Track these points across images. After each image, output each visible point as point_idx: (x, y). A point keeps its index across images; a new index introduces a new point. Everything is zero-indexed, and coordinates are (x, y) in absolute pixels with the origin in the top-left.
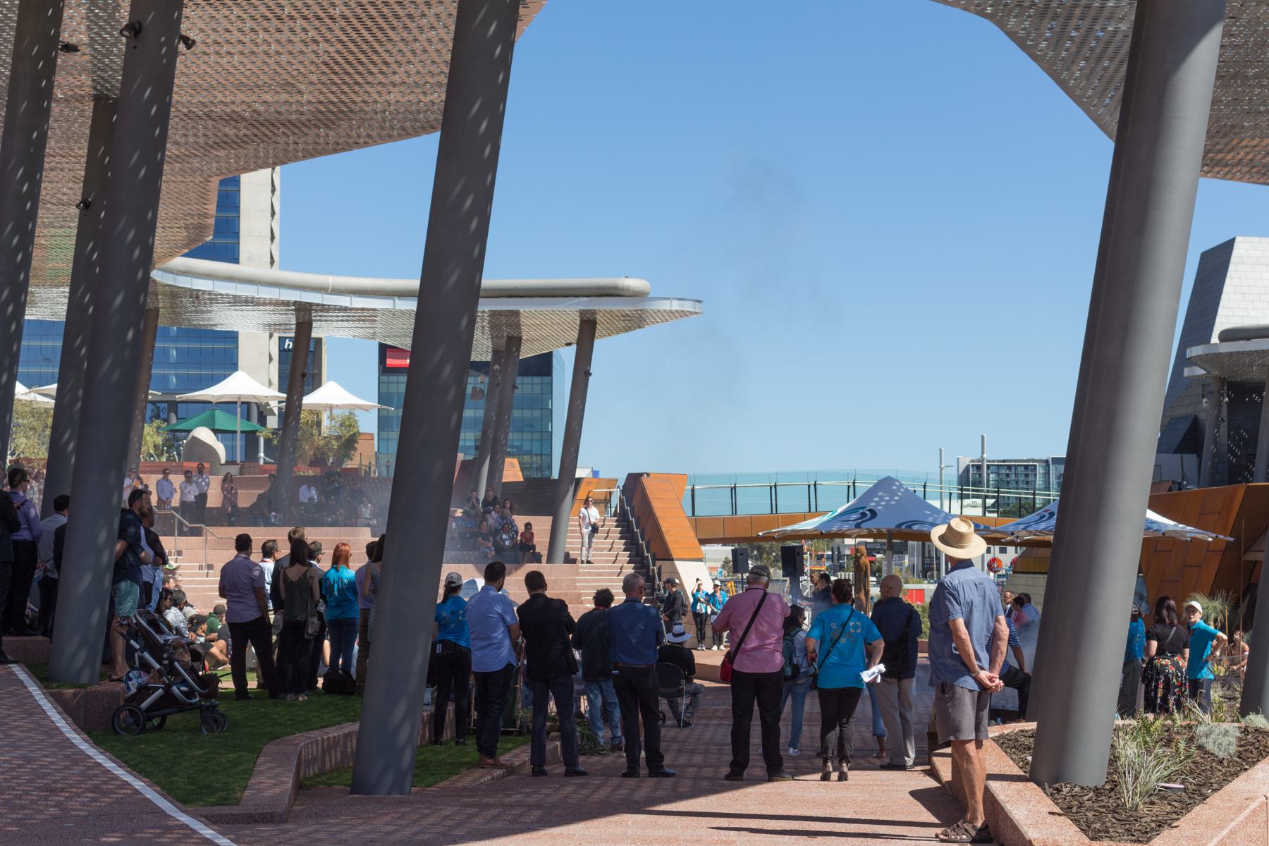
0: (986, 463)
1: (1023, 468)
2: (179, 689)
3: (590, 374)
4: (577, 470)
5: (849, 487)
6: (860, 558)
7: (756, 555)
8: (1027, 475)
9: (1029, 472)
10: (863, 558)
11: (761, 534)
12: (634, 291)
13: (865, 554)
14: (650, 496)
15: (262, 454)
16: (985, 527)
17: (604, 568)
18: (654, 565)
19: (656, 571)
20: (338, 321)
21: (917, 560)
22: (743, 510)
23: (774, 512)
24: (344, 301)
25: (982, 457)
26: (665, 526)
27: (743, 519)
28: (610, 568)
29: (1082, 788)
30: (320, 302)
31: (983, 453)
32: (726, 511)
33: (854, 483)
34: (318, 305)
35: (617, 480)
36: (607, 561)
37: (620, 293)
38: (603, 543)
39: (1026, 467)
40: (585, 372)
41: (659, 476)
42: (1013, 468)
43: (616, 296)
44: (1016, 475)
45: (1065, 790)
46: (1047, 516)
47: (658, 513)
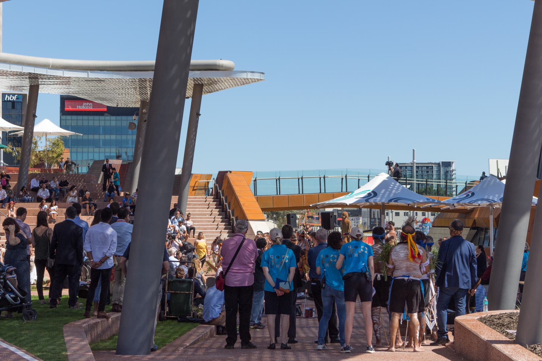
0: (415, 165)
1: (425, 168)
2: (10, 296)
3: (200, 115)
4: (176, 169)
5: (342, 179)
6: (345, 219)
8: (428, 172)
9: (429, 170)
10: (347, 218)
11: (311, 205)
12: (225, 67)
13: (348, 216)
14: (233, 184)
15: (2, 161)
17: (207, 225)
20: (54, 84)
22: (283, 193)
23: (278, 194)
24: (59, 73)
25: (413, 161)
26: (242, 201)
27: (284, 197)
28: (211, 225)
31: (414, 159)
32: (273, 192)
33: (346, 176)
34: (44, 75)
35: (211, 175)
36: (209, 221)
37: (218, 68)
38: (206, 211)
39: (427, 167)
40: (197, 113)
41: (236, 172)
42: (420, 167)
44: (422, 171)
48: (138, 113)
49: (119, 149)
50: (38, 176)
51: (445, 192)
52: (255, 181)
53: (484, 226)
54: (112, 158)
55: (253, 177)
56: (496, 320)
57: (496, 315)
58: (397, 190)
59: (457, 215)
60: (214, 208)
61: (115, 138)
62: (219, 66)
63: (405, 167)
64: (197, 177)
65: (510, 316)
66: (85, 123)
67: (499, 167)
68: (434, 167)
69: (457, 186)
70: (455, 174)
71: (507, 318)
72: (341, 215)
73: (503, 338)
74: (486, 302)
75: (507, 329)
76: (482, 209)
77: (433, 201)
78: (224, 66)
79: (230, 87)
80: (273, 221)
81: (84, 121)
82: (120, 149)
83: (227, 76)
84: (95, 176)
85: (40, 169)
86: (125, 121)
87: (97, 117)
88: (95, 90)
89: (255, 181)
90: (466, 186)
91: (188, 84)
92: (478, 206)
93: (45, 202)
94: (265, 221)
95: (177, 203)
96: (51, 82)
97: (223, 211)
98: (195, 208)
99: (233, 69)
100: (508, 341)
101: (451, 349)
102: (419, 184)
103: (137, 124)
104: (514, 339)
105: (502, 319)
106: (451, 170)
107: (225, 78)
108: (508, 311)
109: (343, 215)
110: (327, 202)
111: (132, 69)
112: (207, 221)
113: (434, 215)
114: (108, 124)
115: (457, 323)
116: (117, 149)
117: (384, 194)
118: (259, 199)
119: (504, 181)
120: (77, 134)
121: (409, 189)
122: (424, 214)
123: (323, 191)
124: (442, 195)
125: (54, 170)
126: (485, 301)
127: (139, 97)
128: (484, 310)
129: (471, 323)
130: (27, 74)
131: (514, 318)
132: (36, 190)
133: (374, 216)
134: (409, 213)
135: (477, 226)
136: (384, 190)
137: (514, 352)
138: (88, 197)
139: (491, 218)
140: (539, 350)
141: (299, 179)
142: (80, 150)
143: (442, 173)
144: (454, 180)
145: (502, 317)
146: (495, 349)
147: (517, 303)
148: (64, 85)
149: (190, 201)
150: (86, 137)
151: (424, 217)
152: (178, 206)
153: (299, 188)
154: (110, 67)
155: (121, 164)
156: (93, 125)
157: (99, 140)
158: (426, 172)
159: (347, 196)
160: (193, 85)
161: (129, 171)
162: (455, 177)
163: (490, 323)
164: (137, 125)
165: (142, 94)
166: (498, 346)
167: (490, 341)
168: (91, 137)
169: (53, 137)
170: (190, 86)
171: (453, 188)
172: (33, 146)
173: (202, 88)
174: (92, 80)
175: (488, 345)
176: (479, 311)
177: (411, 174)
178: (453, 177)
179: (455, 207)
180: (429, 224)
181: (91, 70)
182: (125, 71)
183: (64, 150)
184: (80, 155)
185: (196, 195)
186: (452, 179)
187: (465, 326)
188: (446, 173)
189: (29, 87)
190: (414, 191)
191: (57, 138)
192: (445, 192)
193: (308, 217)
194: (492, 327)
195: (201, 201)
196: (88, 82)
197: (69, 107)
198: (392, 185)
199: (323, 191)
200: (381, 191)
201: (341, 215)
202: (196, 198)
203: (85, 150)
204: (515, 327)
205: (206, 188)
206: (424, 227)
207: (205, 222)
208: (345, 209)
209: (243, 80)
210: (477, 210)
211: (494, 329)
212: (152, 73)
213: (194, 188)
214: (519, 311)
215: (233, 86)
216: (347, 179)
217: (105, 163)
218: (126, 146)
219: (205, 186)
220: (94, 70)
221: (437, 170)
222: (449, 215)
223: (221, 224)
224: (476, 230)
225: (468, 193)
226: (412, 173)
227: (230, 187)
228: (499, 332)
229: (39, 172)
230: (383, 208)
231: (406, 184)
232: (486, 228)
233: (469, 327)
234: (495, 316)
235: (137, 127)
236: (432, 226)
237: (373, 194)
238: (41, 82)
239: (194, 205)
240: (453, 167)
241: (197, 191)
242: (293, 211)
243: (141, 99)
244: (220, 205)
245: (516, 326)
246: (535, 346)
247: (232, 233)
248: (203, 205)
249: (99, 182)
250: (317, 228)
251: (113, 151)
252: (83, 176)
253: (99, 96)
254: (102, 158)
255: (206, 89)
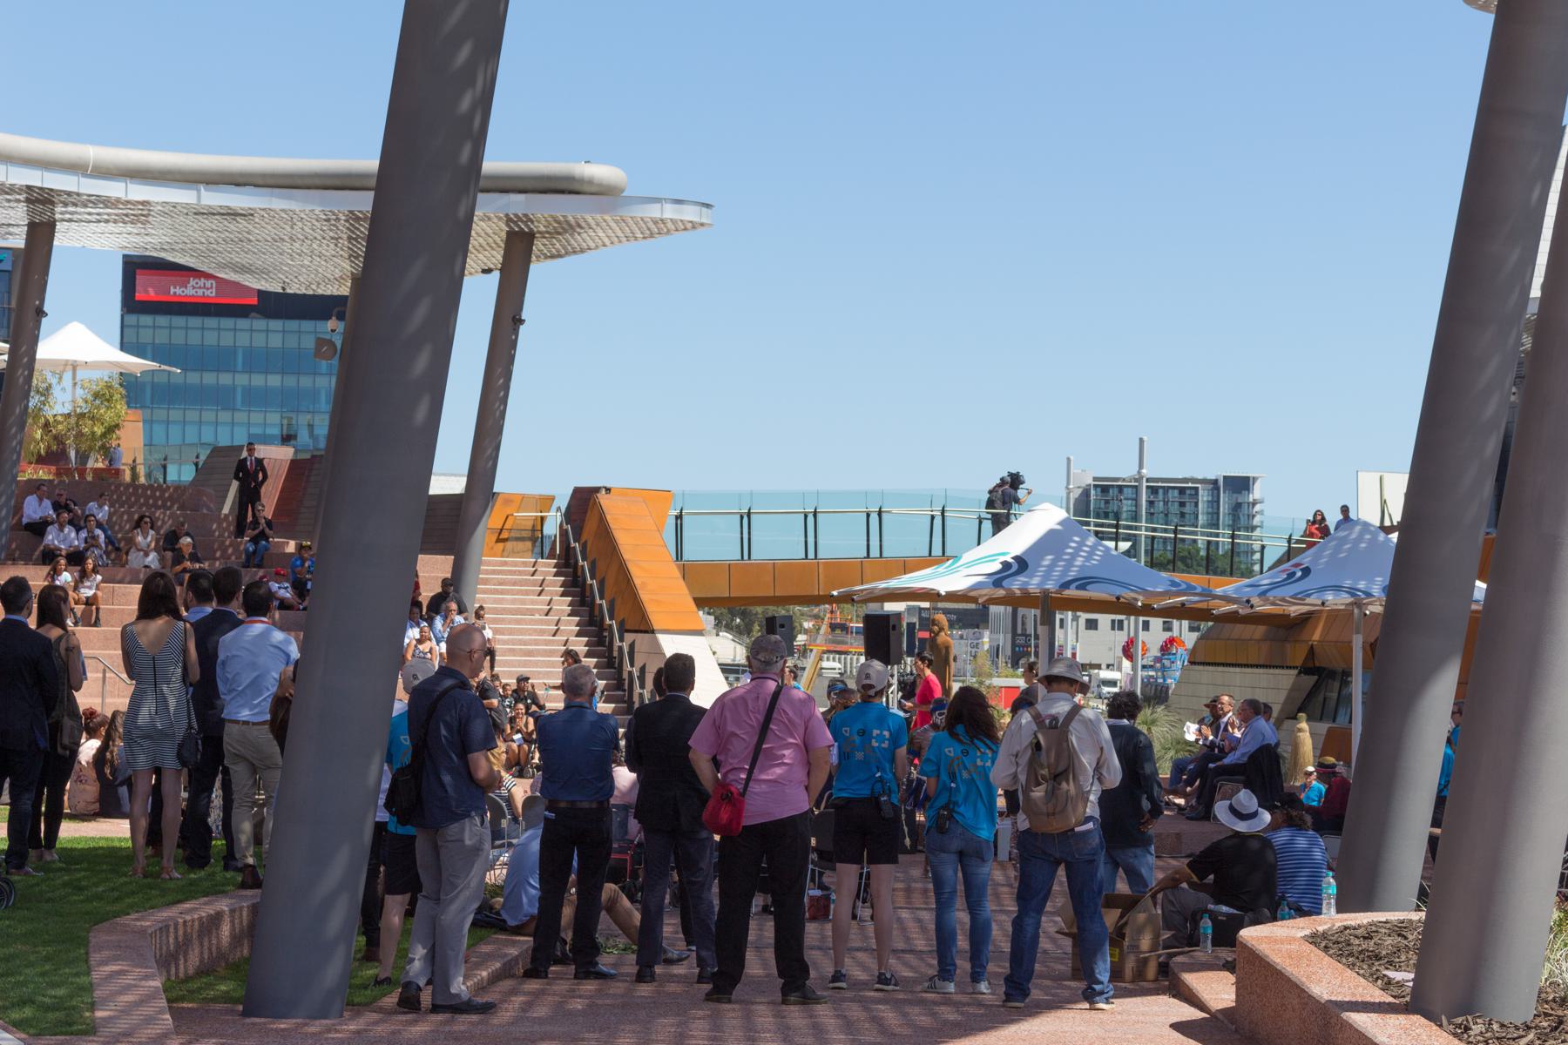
1: (1176, 492)
3: (522, 322)
4: (433, 477)
5: (933, 517)
6: (937, 634)
7: (738, 626)
8: (1182, 504)
9: (1186, 499)
10: (943, 634)
11: (835, 593)
12: (600, 185)
13: (946, 627)
16: (1203, 589)
17: (536, 642)
18: (622, 640)
19: (626, 650)
20: (99, 221)
21: (1004, 640)
22: (759, 554)
23: (746, 557)
24: (114, 189)
25: (1139, 472)
26: (638, 576)
27: (761, 567)
28: (547, 643)
29: (1502, 1026)
30: (74, 189)
31: (1141, 466)
32: (731, 552)
33: (943, 512)
34: (69, 194)
35: (552, 499)
36: (542, 632)
37: (577, 187)
38: (533, 602)
39: (1182, 491)
41: (626, 492)
42: (1161, 491)
43: (562, 192)
44: (1166, 503)
45: (1477, 1029)
46: (1299, 574)
47: (627, 554)
48: (344, 312)
49: (290, 415)
50: (45, 488)
51: (1233, 562)
52: (679, 517)
53: (1339, 666)
54: (267, 440)
55: (672, 507)
56: (1357, 942)
57: (1360, 926)
58: (1088, 558)
59: (1260, 630)
60: (556, 595)
61: (279, 384)
62: (581, 180)
63: (1116, 490)
64: (511, 501)
65: (1400, 929)
66: (194, 338)
67: (1386, 497)
68: (1200, 492)
69: (1263, 547)
70: (1261, 512)
71: (1389, 935)
72: (928, 623)
73: (1376, 995)
74: (1330, 886)
75: (1387, 969)
76: (1334, 615)
77: (1190, 590)
78: (595, 181)
79: (612, 243)
80: (731, 637)
81: (174, 332)
82: (293, 415)
83: (603, 212)
84: (213, 492)
85: (53, 469)
86: (306, 333)
87: (227, 322)
88: (220, 240)
89: (679, 517)
90: (1289, 547)
91: (473, 233)
92: (1322, 608)
93: (63, 561)
94: (703, 635)
95: (449, 576)
96: (89, 214)
97: (582, 603)
98: (502, 592)
99: (623, 191)
100: (1389, 1003)
101: (1226, 1021)
102: (1153, 538)
103: (339, 344)
104: (1408, 999)
105: (1376, 939)
106: (1251, 500)
107: (598, 217)
108: (1394, 916)
109: (934, 622)
110: (882, 585)
111: (329, 182)
112: (535, 630)
113: (1197, 629)
114: (259, 341)
115: (1244, 946)
116: (284, 415)
117: (1051, 567)
118: (688, 571)
119: (1394, 536)
120: (164, 367)
121: (1127, 553)
122: (1167, 628)
123: (875, 552)
124: (1223, 573)
125: (96, 471)
126: (1329, 883)
127: (347, 265)
128: (1324, 911)
129: (1286, 947)
130: (21, 190)
131: (1411, 937)
132: (38, 528)
133: (1024, 629)
134: (1126, 623)
135: (1317, 664)
136: (1050, 557)
137: (1404, 1036)
138: (187, 551)
139: (1358, 642)
140: (1478, 1032)
141: (806, 517)
142: (175, 415)
143: (1224, 509)
144: (1258, 529)
145: (1377, 932)
146: (1351, 1025)
147: (1423, 894)
148: (129, 225)
149: (487, 572)
150: (193, 378)
151: (1168, 635)
152: (451, 590)
153: (816, 537)
154: (264, 175)
155: (292, 460)
156: (216, 343)
157: (234, 388)
158: (1177, 504)
159: (941, 569)
160: (504, 235)
161: (312, 479)
162: (1262, 522)
163: (1340, 950)
164: (339, 347)
165: (355, 258)
166: (1360, 1020)
167: (1336, 1003)
168: (209, 378)
169: (96, 375)
170: (496, 238)
171: (1253, 552)
172: (34, 401)
173: (532, 244)
174: (211, 213)
175: (1329, 1015)
176: (1301, 912)
177: (1134, 509)
178: (1256, 521)
179: (1252, 607)
180: (1181, 656)
181: (207, 184)
182: (308, 188)
183: (126, 413)
184: (175, 431)
185: (505, 553)
186: (1253, 528)
187: (1267, 956)
188: (1236, 508)
189: (26, 228)
190: (1139, 561)
191: (106, 379)
192: (1233, 562)
193: (833, 627)
194: (1344, 960)
195: (519, 571)
196: (238, 219)
197: (148, 289)
198: (1073, 545)
199: (875, 552)
200: (1042, 559)
201: (928, 623)
202: (505, 563)
203: (192, 415)
204: (1411, 962)
205: (534, 537)
206: (1166, 663)
207: (530, 635)
208: (941, 605)
209: (653, 226)
210: (1319, 618)
211: (1351, 966)
212: (370, 196)
213: (500, 534)
214: (1423, 915)
215: (620, 242)
216: (947, 519)
217: (245, 454)
218: (311, 406)
219: (533, 530)
220: (218, 184)
221: (1210, 499)
222: (1239, 630)
223: (576, 641)
224: (1316, 677)
225: (1293, 569)
226: (1136, 506)
227: (605, 531)
228: (1364, 976)
229: (51, 477)
230: (1049, 605)
231: (1116, 538)
232: (1343, 671)
233: (1278, 961)
234: (1355, 929)
235: (339, 352)
236: (1189, 662)
237: (1015, 567)
238: (61, 213)
239: (501, 584)
240: (1257, 492)
241: (509, 545)
242: (791, 607)
243: (352, 273)
244: (575, 586)
245: (1414, 959)
246: (1467, 1021)
247: (608, 668)
248: (526, 583)
249: (226, 510)
250: (858, 659)
251: (273, 421)
252: (179, 488)
253: (232, 259)
254: (241, 439)
255: (543, 248)
